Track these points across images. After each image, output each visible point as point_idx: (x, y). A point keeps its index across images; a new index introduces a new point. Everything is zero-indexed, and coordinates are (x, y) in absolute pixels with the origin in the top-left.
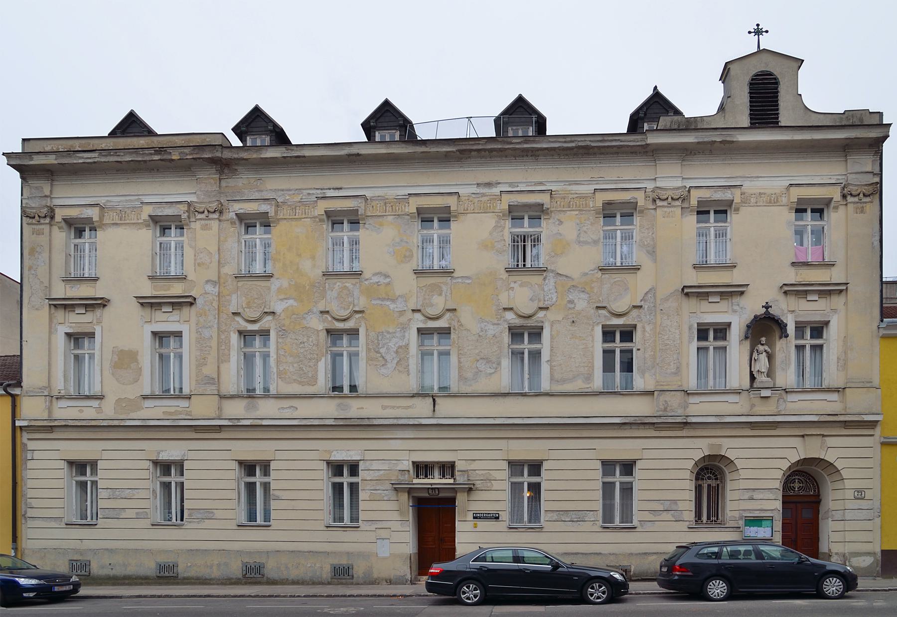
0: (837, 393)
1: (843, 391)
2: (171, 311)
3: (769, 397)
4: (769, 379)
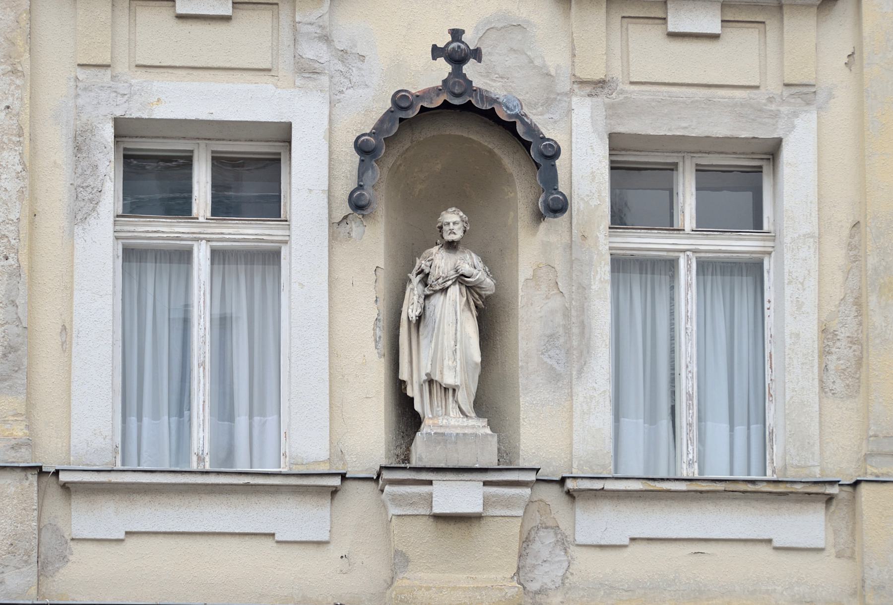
0: (821, 507)
1: (853, 500)
4: (480, 426)
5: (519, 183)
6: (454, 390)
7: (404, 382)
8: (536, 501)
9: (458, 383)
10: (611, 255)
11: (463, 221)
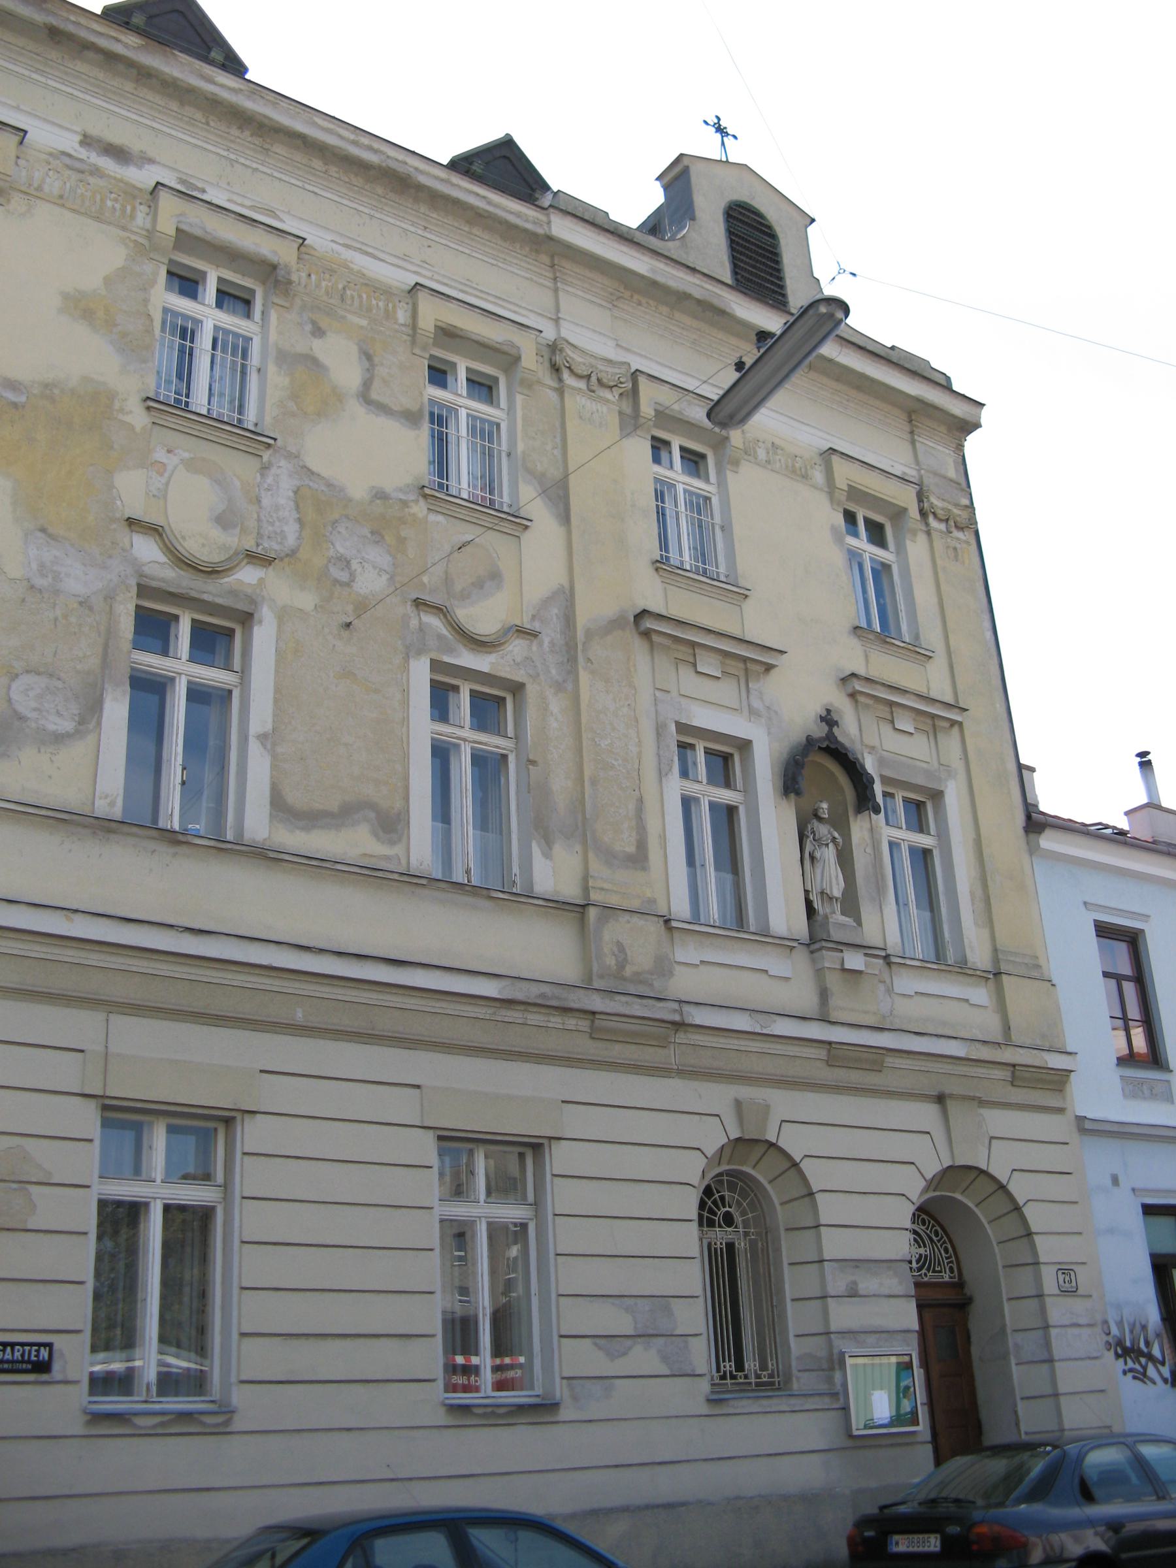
3: (860, 972)
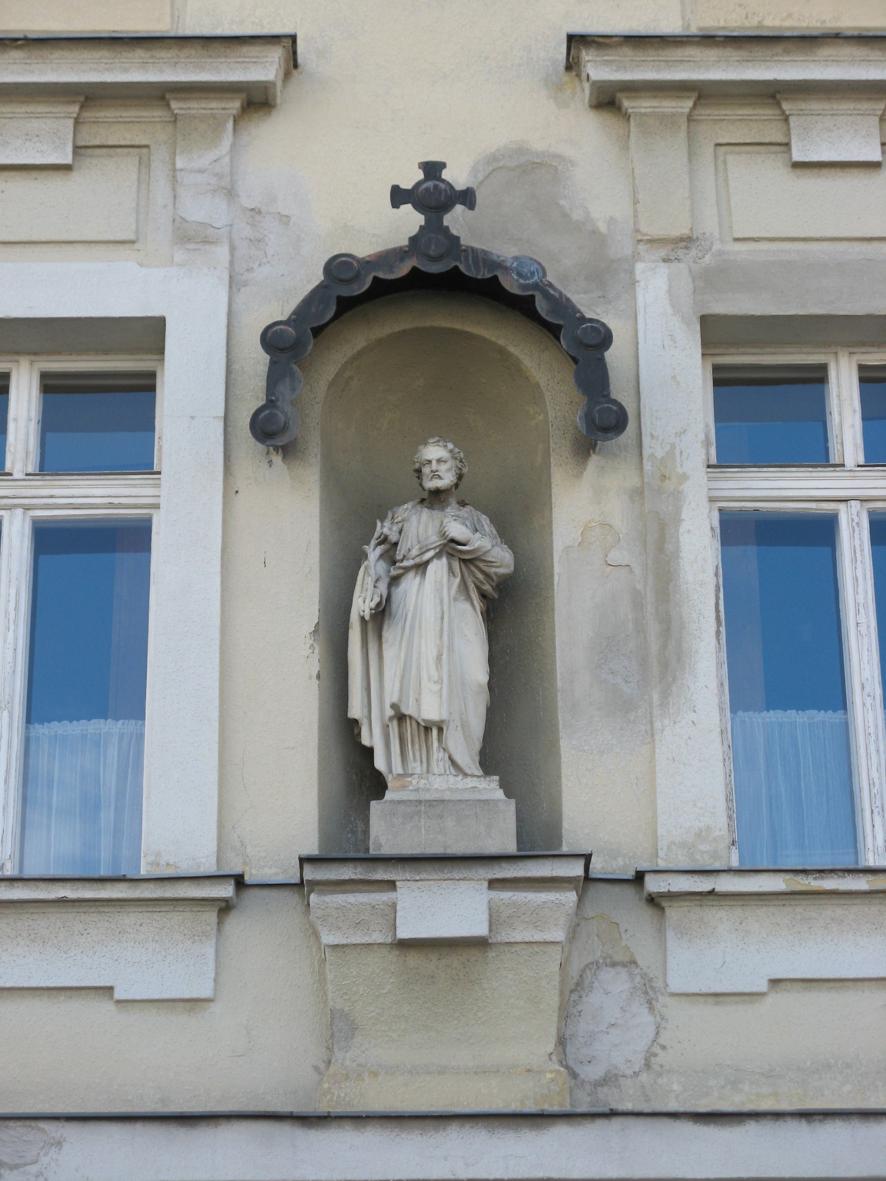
2: (68, 159)
5: (551, 397)
6: (440, 730)
7: (356, 722)
8: (593, 918)
9: (445, 716)
10: (720, 510)
11: (456, 459)
